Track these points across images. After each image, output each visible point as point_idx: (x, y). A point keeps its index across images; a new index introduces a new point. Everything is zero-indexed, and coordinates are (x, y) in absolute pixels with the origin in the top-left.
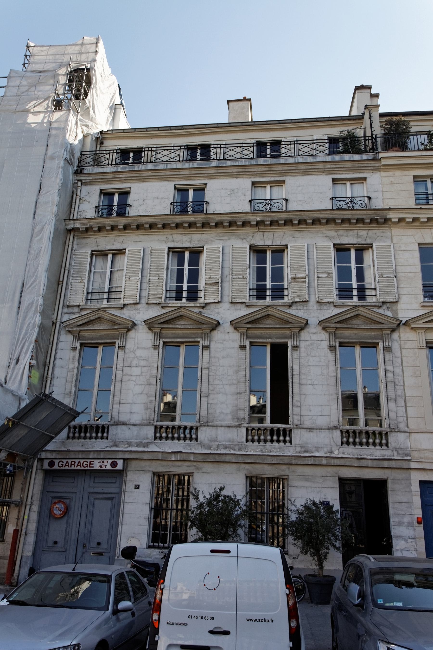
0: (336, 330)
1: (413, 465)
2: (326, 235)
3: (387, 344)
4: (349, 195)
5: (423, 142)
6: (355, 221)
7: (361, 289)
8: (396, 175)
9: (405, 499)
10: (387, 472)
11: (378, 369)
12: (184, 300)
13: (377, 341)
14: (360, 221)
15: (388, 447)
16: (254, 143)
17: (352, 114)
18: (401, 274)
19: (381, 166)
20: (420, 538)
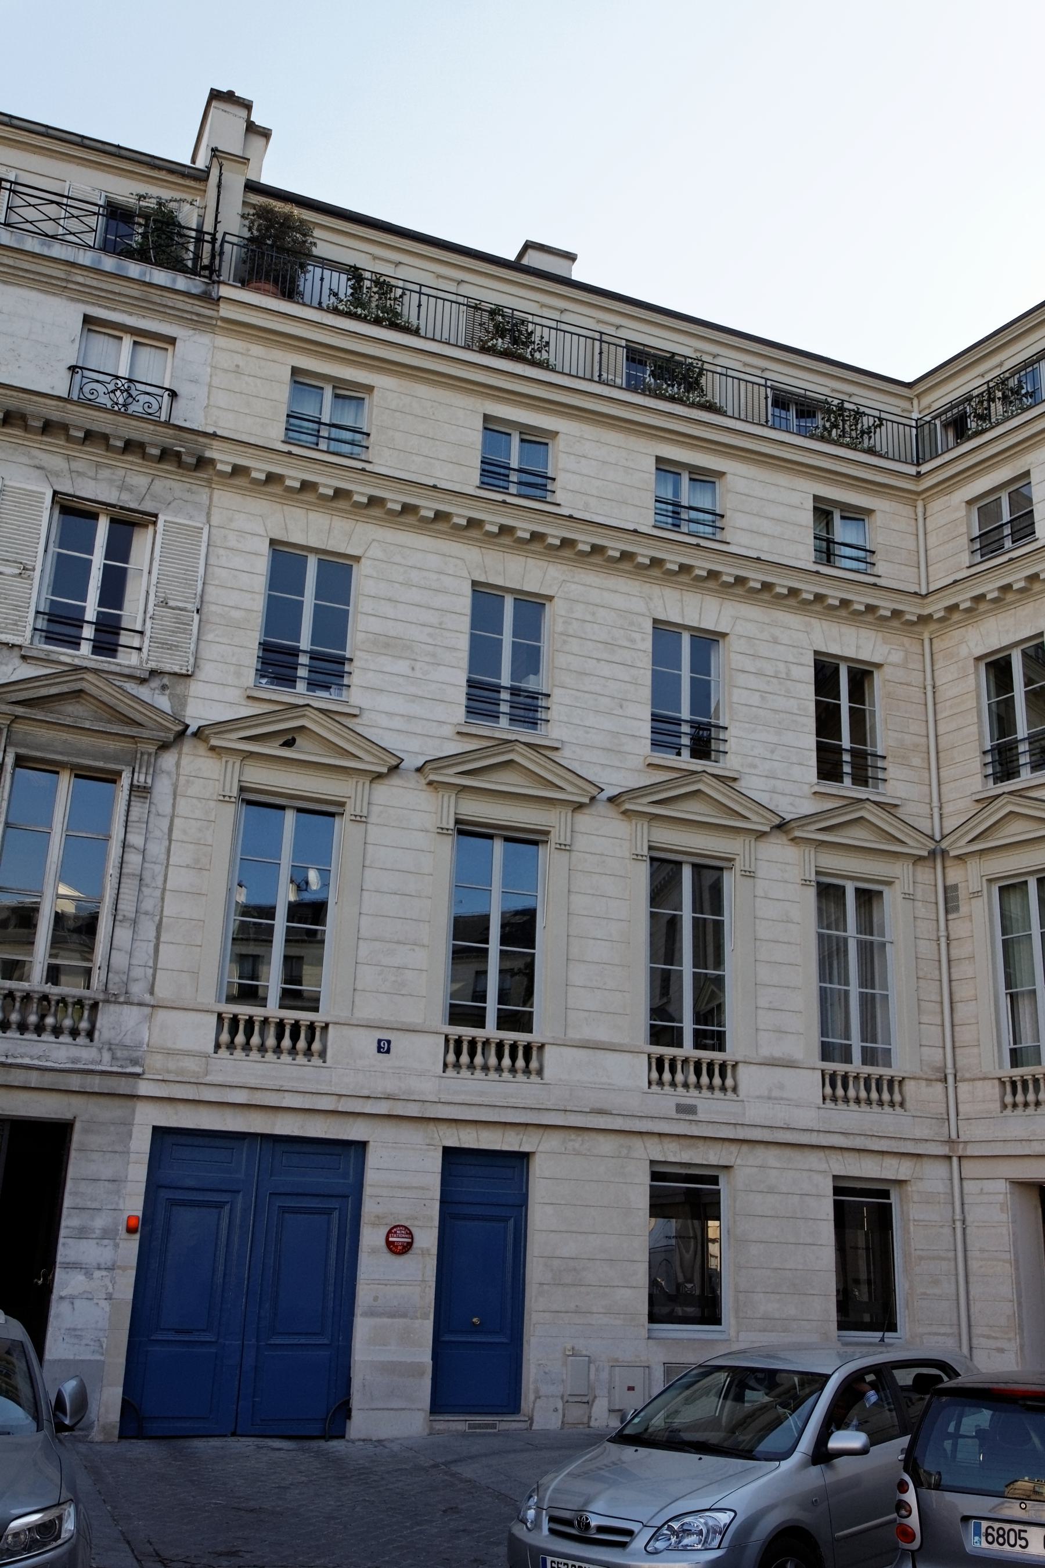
0: (12, 722)
1: (144, 1088)
2: (37, 462)
3: (142, 779)
4: (123, 372)
5: (335, 287)
6: (120, 444)
7: (105, 625)
8: (250, 353)
9: (107, 1173)
10: (77, 1101)
11: (107, 838)
12: (301, 687)
13: (118, 767)
14: (131, 447)
15: (92, 1041)
18: (213, 608)
19: (217, 319)
20: (124, 1269)
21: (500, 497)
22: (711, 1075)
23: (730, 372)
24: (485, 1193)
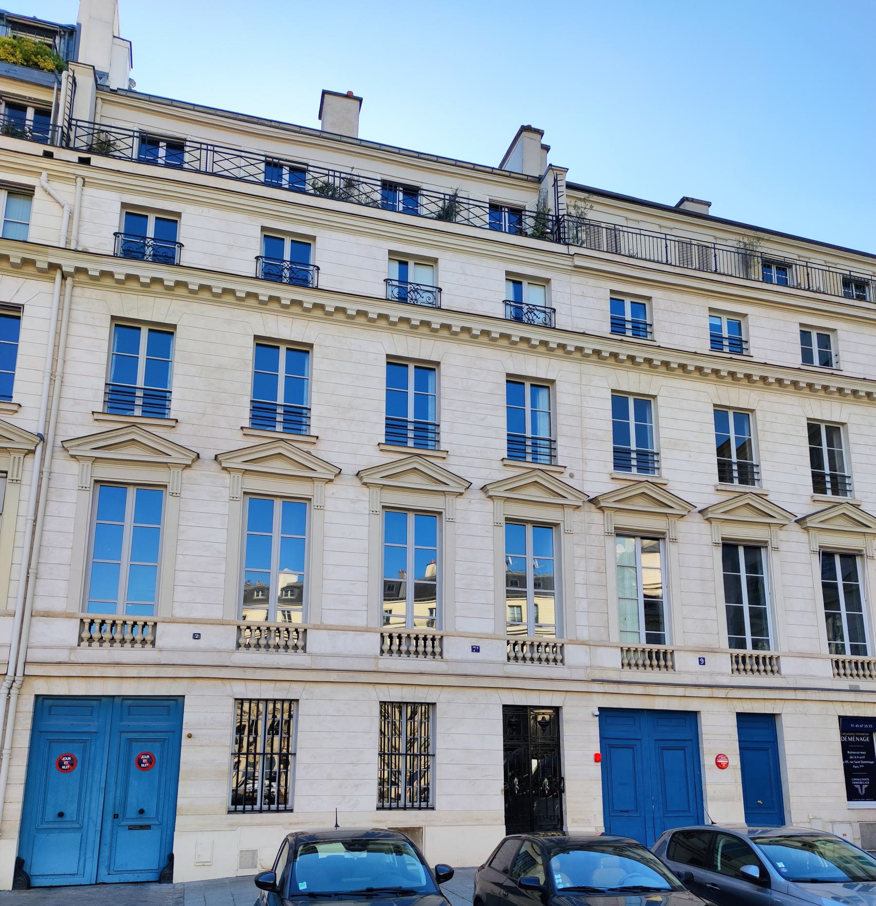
16: (134, 131)
17: (507, 167)
21: (619, 338)
22: (658, 659)
23: (643, 232)
24: (759, 735)
